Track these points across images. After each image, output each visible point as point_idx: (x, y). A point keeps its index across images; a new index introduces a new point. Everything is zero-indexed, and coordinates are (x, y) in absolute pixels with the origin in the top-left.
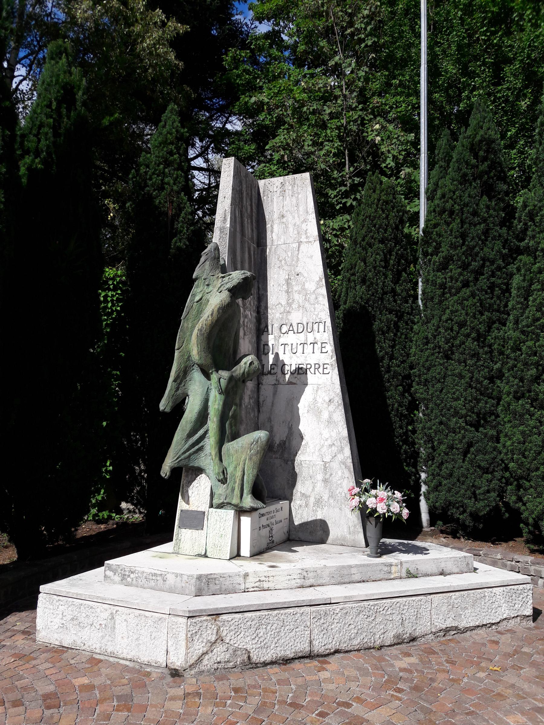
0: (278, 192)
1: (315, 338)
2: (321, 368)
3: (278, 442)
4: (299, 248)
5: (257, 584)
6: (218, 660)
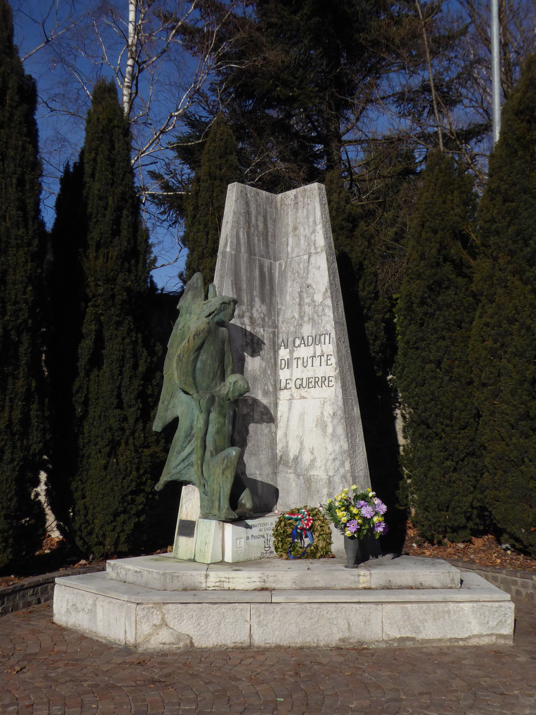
0: (292, 205)
1: (322, 351)
2: (327, 381)
3: (292, 458)
4: (309, 259)
5: (217, 584)
6: (164, 641)
